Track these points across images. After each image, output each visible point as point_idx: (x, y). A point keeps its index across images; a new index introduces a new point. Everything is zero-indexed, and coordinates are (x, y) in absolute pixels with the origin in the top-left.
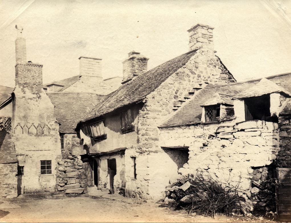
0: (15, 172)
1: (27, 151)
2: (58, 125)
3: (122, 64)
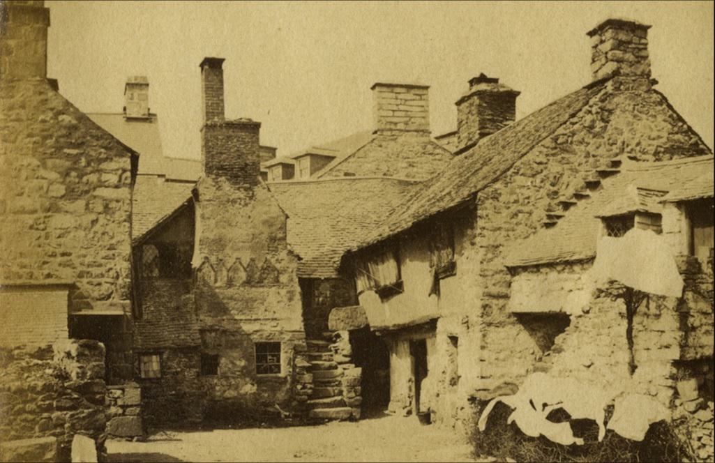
0: (195, 368)
1: (641, 356)
2: (296, 259)
3: (455, 107)
